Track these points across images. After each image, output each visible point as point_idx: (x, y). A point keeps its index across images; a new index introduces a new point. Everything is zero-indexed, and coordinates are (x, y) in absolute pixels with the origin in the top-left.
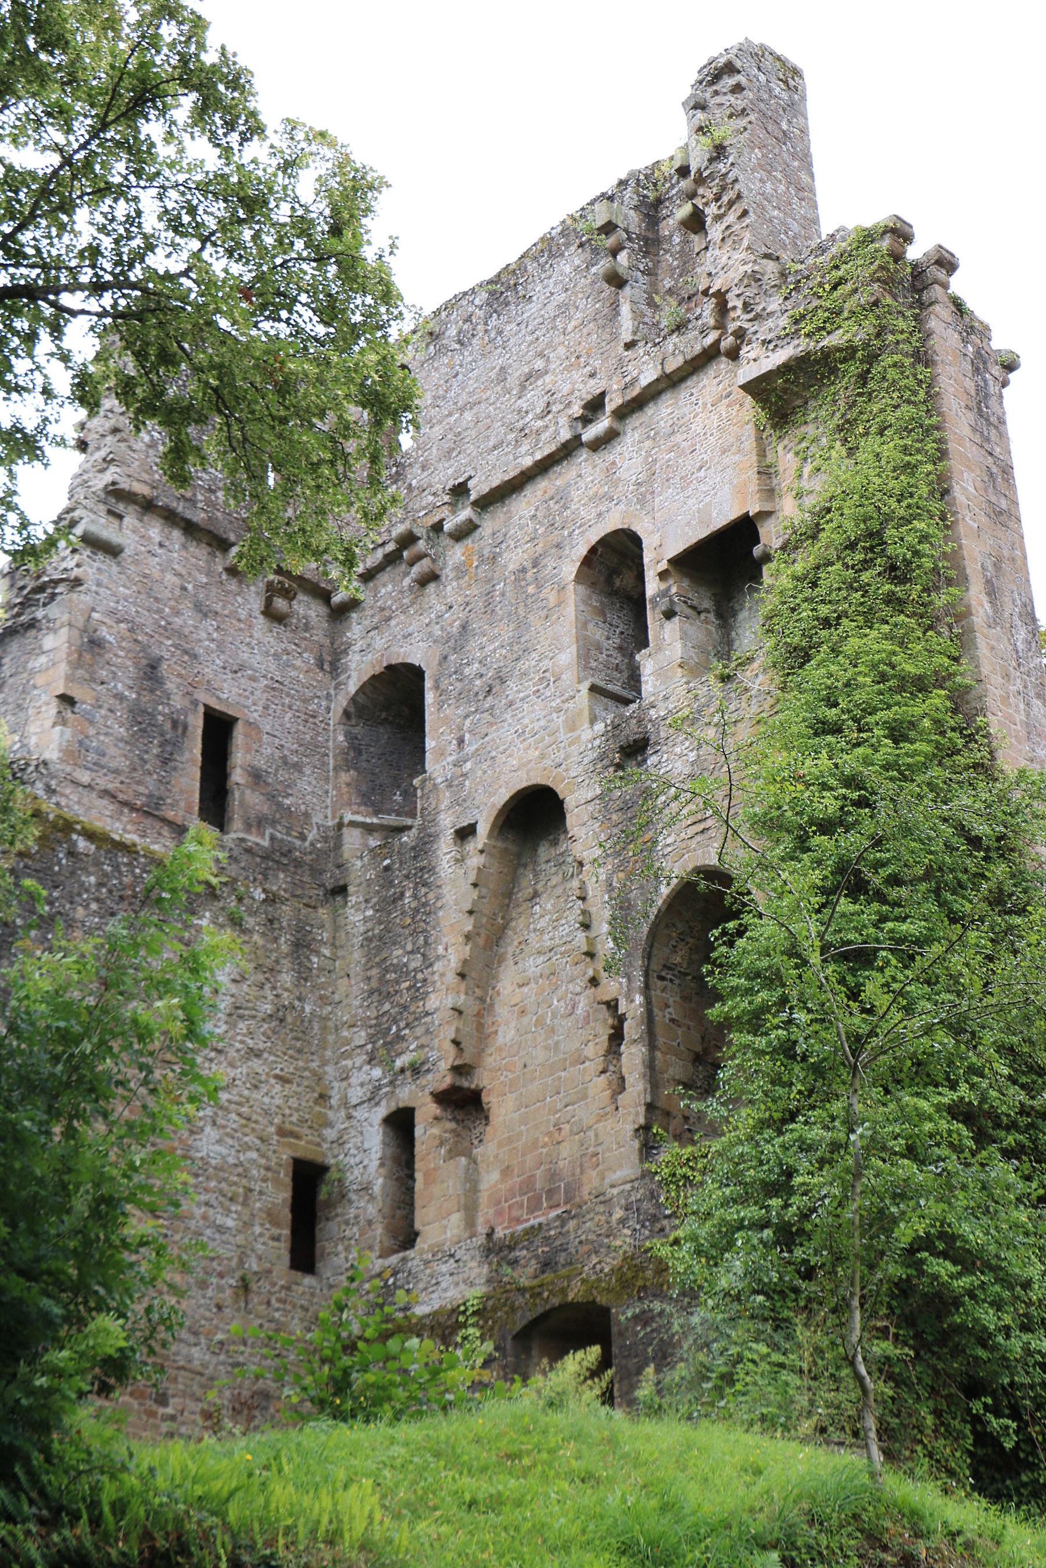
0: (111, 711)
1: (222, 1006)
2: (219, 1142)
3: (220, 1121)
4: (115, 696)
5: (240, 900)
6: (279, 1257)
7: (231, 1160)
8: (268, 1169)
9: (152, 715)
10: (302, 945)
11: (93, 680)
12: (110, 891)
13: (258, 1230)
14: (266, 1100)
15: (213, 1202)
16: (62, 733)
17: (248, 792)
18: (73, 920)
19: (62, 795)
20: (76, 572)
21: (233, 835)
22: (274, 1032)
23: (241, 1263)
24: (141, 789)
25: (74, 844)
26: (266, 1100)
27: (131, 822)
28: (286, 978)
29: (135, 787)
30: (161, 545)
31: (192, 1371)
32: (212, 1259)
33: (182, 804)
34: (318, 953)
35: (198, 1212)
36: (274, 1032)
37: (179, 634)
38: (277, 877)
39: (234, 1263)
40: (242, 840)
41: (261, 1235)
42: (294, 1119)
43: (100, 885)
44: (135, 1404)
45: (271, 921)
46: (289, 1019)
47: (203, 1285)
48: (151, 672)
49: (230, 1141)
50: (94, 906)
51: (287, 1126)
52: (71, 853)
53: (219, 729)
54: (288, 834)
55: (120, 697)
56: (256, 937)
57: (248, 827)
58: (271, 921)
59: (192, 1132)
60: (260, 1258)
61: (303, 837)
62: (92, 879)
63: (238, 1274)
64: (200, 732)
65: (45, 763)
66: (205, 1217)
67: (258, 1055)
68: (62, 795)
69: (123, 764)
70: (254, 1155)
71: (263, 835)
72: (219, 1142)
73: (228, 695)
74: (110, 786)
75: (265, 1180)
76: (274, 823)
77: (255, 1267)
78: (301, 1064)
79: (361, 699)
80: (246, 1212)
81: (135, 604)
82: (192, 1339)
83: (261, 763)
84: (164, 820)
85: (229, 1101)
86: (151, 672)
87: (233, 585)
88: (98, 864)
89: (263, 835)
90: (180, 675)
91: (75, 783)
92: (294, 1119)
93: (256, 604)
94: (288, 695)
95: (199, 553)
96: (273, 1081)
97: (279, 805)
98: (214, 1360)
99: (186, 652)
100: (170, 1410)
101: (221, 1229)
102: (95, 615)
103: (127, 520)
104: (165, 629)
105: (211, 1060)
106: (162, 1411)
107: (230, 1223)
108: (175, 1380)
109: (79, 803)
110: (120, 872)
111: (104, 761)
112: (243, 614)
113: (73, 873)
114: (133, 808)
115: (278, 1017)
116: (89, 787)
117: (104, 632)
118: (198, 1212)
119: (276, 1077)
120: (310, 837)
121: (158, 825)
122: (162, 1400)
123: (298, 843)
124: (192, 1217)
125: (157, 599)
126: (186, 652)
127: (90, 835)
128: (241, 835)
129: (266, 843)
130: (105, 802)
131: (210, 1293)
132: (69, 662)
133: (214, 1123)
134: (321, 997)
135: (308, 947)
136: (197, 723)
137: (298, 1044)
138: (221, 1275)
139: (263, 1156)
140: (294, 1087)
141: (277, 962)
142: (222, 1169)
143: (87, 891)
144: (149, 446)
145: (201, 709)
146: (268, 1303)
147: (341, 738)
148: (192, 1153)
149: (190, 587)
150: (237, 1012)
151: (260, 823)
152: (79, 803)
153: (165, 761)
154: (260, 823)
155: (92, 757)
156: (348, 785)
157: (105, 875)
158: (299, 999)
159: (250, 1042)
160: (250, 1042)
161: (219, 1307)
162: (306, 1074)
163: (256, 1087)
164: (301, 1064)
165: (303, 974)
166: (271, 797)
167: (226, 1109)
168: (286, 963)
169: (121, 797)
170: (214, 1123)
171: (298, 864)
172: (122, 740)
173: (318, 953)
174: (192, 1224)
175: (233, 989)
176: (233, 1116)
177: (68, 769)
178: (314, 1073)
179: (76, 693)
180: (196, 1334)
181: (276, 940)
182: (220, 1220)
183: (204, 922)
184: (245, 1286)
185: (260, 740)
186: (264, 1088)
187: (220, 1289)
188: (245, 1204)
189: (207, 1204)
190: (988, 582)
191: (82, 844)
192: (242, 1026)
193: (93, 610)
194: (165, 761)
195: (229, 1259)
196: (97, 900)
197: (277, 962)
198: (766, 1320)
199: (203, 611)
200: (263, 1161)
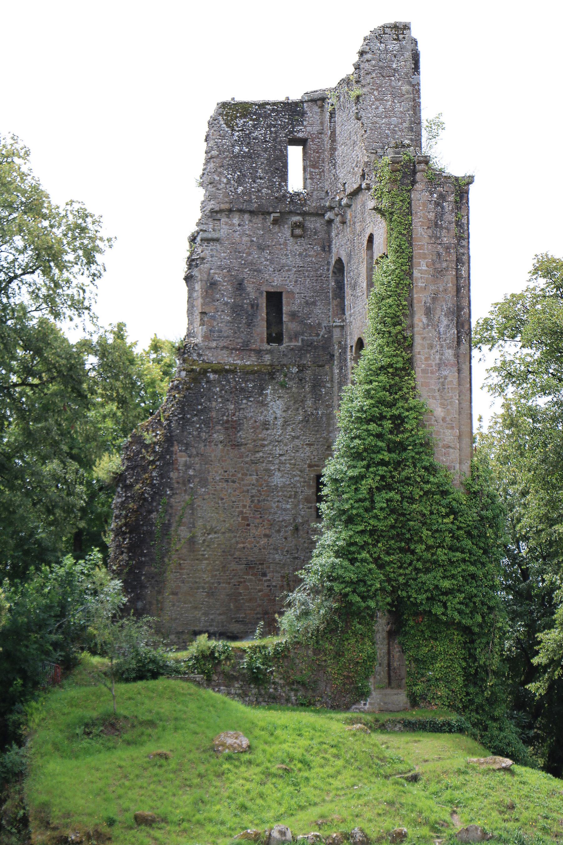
0: (223, 311)
1: (279, 423)
2: (282, 477)
3: (282, 469)
4: (224, 304)
5: (285, 376)
6: (311, 515)
7: (288, 483)
8: (305, 482)
9: (242, 306)
10: (317, 385)
11: (214, 301)
12: (226, 392)
13: (301, 506)
14: (302, 455)
15: (281, 500)
16: (202, 329)
17: (289, 324)
18: (211, 408)
19: (205, 355)
20: (202, 255)
21: (284, 345)
22: (304, 427)
23: (294, 520)
24: (240, 340)
25: (209, 377)
26: (302, 455)
27: (237, 355)
28: (309, 403)
29: (236, 340)
30: (239, 225)
31: (276, 563)
32: (282, 522)
33: (258, 340)
34: (325, 387)
35: (274, 506)
36: (304, 427)
37: (252, 263)
38: (306, 356)
39: (291, 521)
40: (288, 346)
41: (303, 508)
42: (316, 460)
43: (221, 390)
44: (253, 578)
45: (301, 380)
46: (311, 420)
47: (279, 531)
48: (240, 286)
49: (287, 476)
50: (219, 400)
51: (313, 463)
52: (208, 382)
53: (275, 299)
54: (311, 336)
55: (226, 304)
56: (294, 389)
57: (290, 340)
58: (301, 380)
59: (269, 476)
60: (303, 517)
61: (318, 335)
62: (218, 389)
63: (294, 524)
64: (265, 305)
65: (196, 345)
66: (277, 507)
67: (298, 438)
68: (205, 355)
69: (231, 332)
70: (298, 478)
71: (298, 341)
72: (282, 477)
73: (277, 282)
74: (225, 344)
75: (304, 486)
76: (302, 334)
77: (300, 521)
78: (318, 436)
79: (337, 266)
80: (296, 500)
81: (229, 259)
82: (275, 552)
83: (295, 308)
84: (251, 350)
85: (285, 460)
86: (240, 286)
87: (276, 229)
88: (220, 382)
89: (298, 341)
90: (253, 283)
91: (210, 348)
92: (316, 460)
93: (288, 233)
94: (307, 271)
95: (258, 221)
96: (305, 446)
97: (306, 324)
98: (285, 558)
99: (255, 271)
100: (268, 578)
101: (285, 510)
102: (212, 271)
103: (222, 220)
104: (245, 264)
105: (276, 446)
106: (265, 578)
107: (288, 506)
108: (269, 567)
109: (212, 356)
110: (230, 383)
111: (221, 334)
112: (282, 241)
113: (209, 389)
114: (236, 350)
115: (306, 420)
116: (217, 347)
117: (217, 278)
118: (274, 506)
119: (307, 444)
120: (322, 333)
121: (248, 353)
122: (264, 575)
123: (315, 338)
124: (272, 507)
125: (239, 252)
126: (255, 271)
127: (215, 372)
128: (287, 344)
129: (300, 344)
130: (224, 351)
131: (282, 534)
132: (202, 297)
133: (279, 470)
134: (327, 406)
135: (320, 386)
136: (263, 302)
137: (316, 429)
138: (286, 527)
139: (302, 477)
140: (316, 447)
141: (305, 397)
142: (284, 487)
143: (216, 394)
144: (227, 184)
145: (265, 294)
146: (308, 533)
147: (333, 284)
148: (270, 484)
149: (255, 239)
150: (286, 423)
151: (295, 336)
152: (212, 356)
153: (249, 324)
154: (295, 336)
155: (216, 334)
156: (336, 306)
157: (223, 385)
158: (315, 410)
159: (293, 434)
160: (293, 434)
161: (286, 538)
162: (321, 439)
163: (297, 451)
164: (318, 436)
165: (317, 397)
166: (302, 322)
167: (285, 463)
168: (309, 396)
169: (230, 347)
170: (279, 470)
171: (316, 348)
172: (229, 322)
173: (325, 387)
174: (272, 511)
175: (284, 414)
176: (288, 465)
177: (206, 344)
178: (324, 438)
179: (206, 310)
180: (277, 550)
181: (304, 387)
182: (284, 506)
183: (269, 391)
184: (297, 529)
185: (294, 297)
186: (301, 451)
187: (286, 532)
188: (295, 498)
189: (278, 501)
190: (120, 675)
191: (212, 376)
192: (289, 428)
193: (211, 269)
194: (249, 324)
195: (290, 520)
196: (221, 397)
197: (305, 397)
198: (480, 548)
199: (261, 248)
200: (302, 480)
